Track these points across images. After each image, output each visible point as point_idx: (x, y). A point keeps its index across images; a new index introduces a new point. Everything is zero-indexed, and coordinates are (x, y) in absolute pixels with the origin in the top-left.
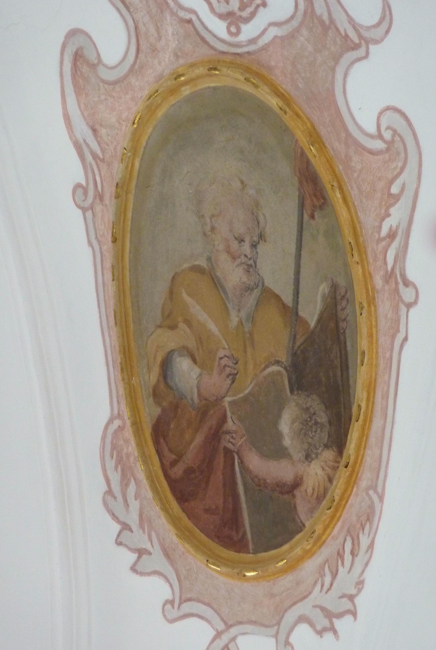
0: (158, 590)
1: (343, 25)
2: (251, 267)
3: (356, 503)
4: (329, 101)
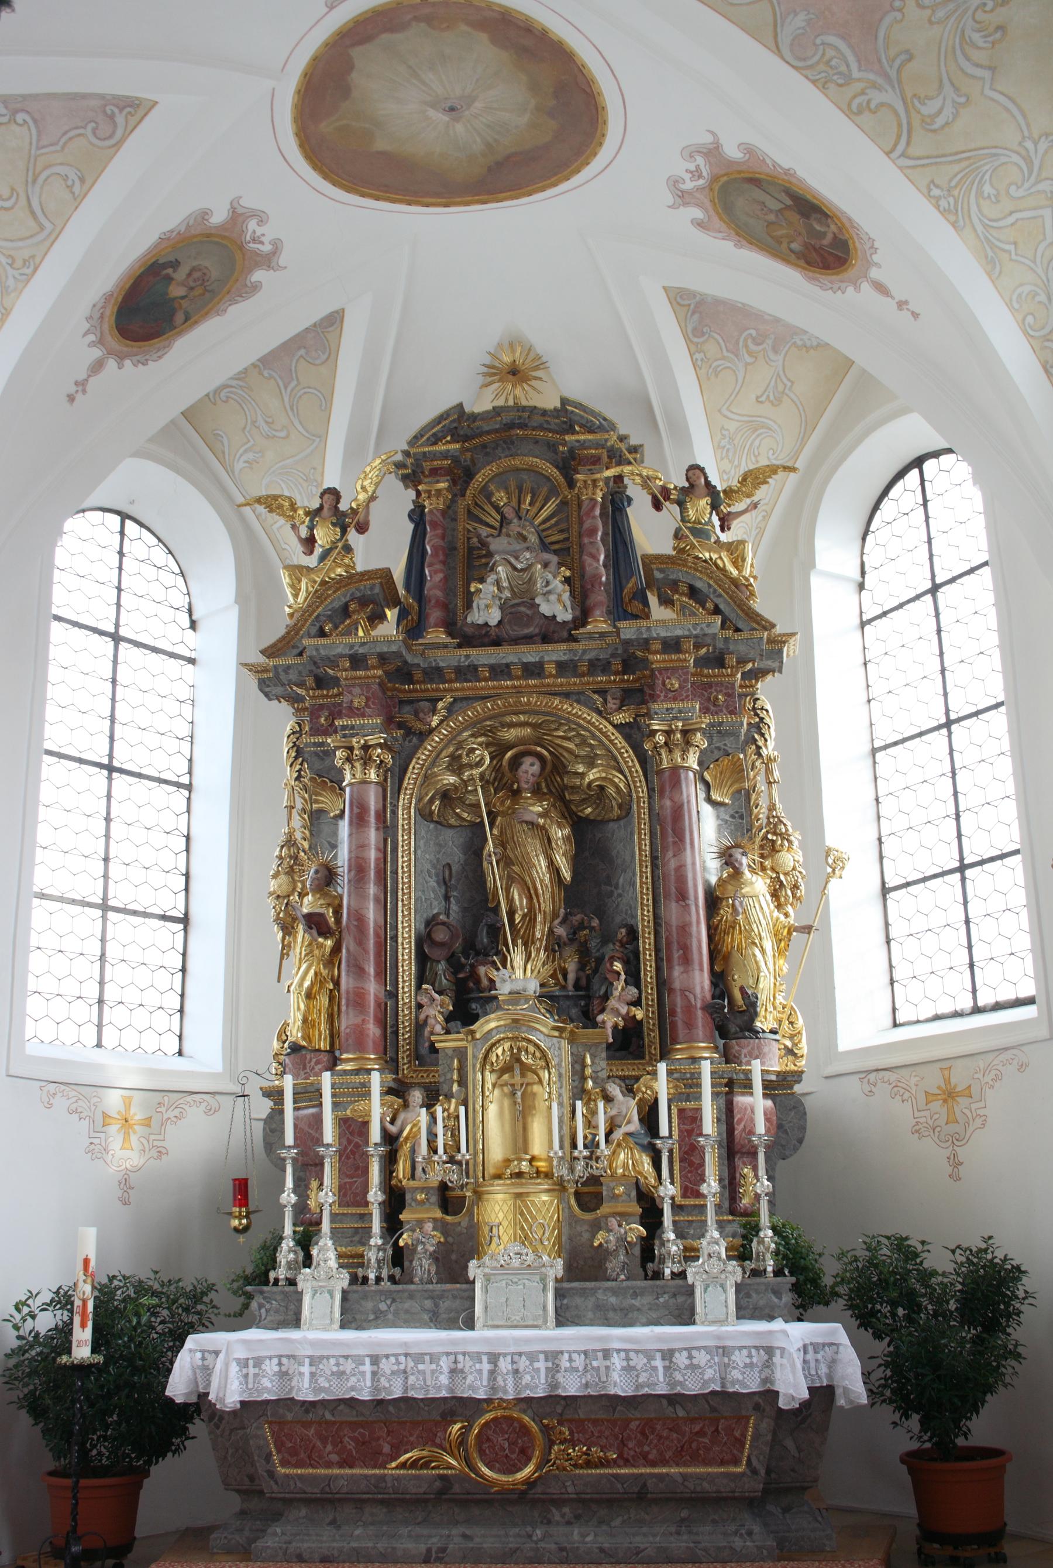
0: (850, 289)
1: (711, 146)
2: (771, 211)
3: (844, 220)
4: (731, 163)
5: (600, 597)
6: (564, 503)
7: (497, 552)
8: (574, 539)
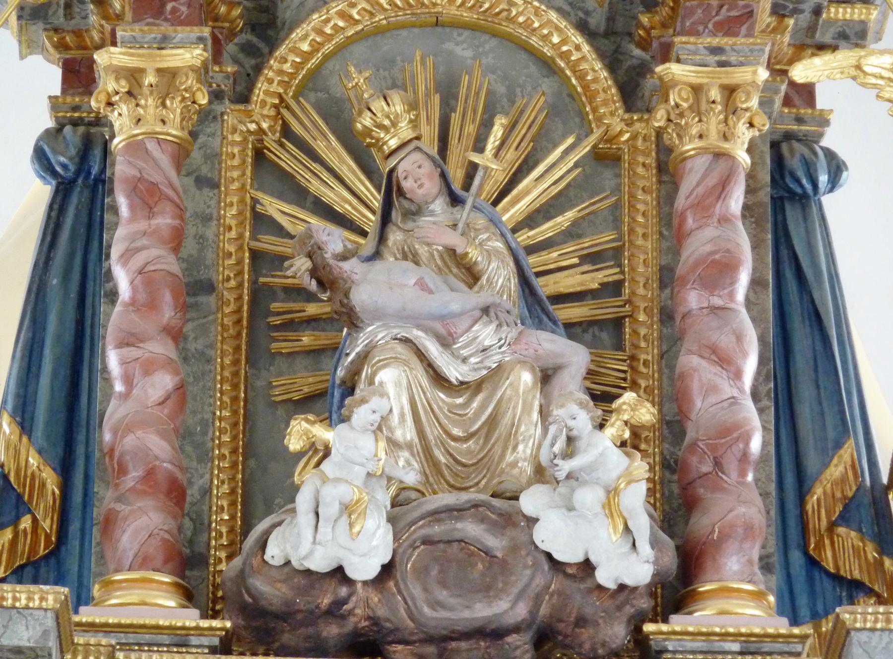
5: (741, 507)
6: (605, 157)
7: (378, 315)
8: (642, 289)
